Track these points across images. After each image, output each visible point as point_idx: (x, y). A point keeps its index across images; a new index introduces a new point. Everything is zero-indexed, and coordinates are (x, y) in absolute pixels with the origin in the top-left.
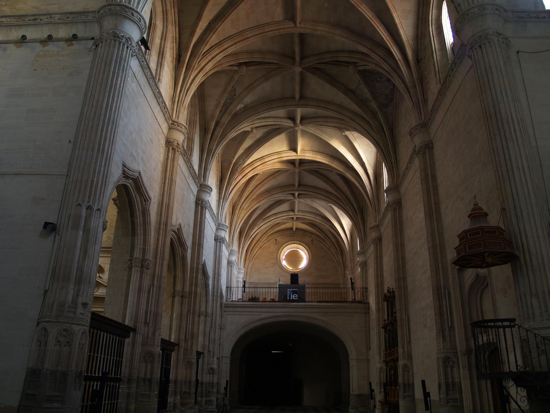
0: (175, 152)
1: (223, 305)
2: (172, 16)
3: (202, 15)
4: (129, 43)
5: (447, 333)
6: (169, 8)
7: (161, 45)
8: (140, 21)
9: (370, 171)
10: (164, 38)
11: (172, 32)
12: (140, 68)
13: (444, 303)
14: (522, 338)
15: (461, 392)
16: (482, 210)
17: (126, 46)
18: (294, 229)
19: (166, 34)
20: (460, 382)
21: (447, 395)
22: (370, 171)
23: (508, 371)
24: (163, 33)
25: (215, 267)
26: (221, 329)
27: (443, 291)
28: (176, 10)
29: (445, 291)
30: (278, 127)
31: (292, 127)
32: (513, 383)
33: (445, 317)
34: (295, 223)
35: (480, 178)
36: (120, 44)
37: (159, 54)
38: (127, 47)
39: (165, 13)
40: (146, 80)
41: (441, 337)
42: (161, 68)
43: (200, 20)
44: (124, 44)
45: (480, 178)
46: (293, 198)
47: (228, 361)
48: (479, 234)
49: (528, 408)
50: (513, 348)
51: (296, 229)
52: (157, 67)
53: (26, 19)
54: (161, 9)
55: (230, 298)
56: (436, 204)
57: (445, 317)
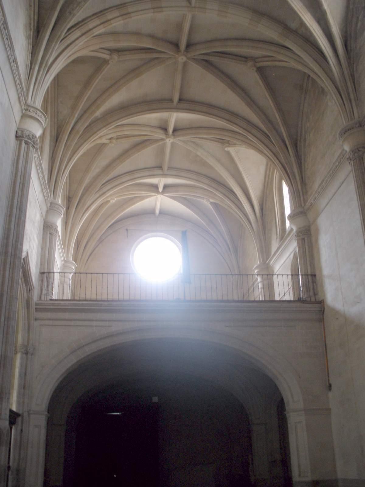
0: (28, 148)
1: (33, 307)
9: (336, 30)
18: (157, 212)
22: (336, 30)
25: (14, 192)
26: (27, 353)
30: (145, 138)
31: (162, 139)
34: (160, 197)
46: (163, 137)
47: (41, 421)
51: (161, 213)
55: (47, 294)
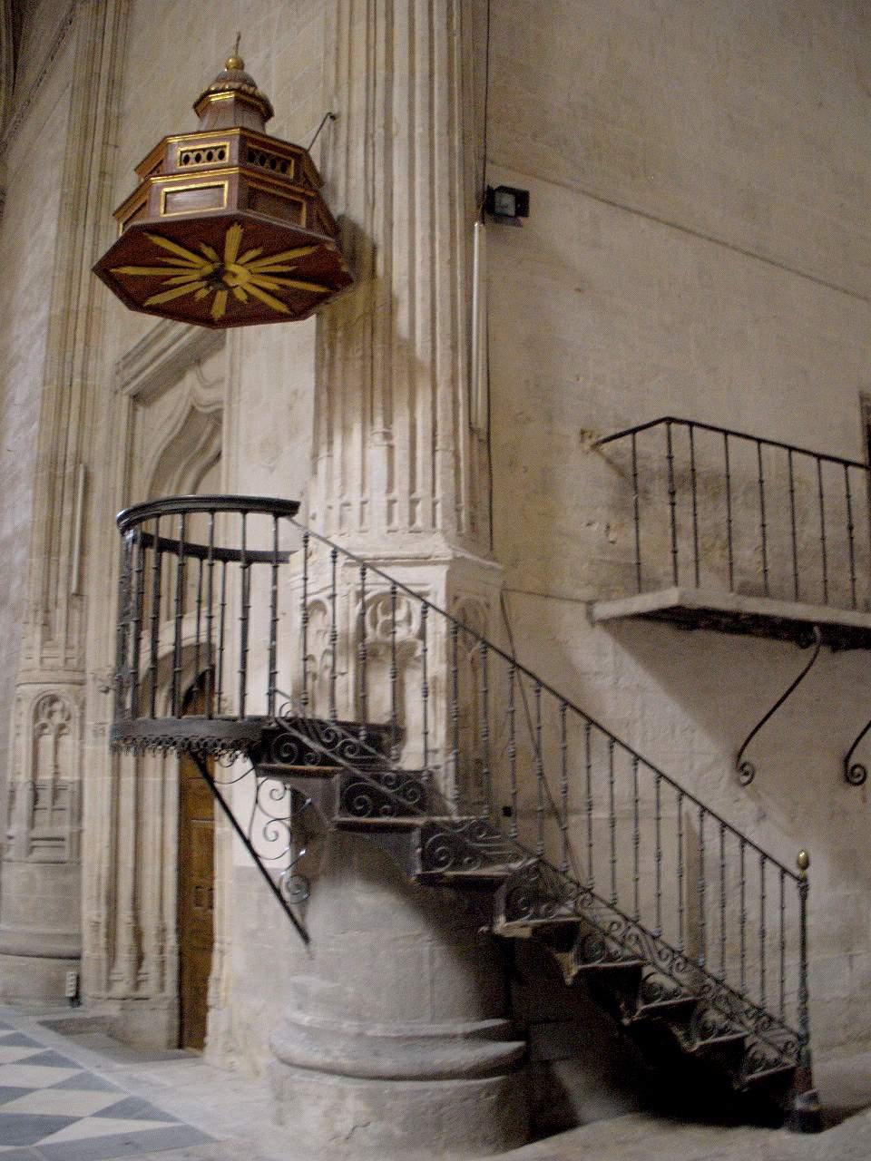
3: (111, 825)
5: (59, 615)
13: (67, 511)
14: (310, 599)
15: (78, 816)
16: (252, 84)
20: (81, 783)
21: (32, 824)
23: (236, 713)
27: (70, 469)
29: (76, 469)
32: (248, 765)
33: (64, 559)
35: (268, 56)
41: (38, 629)
45: (268, 56)
48: (222, 156)
49: (286, 862)
50: (266, 655)
56: (102, 174)
57: (64, 559)
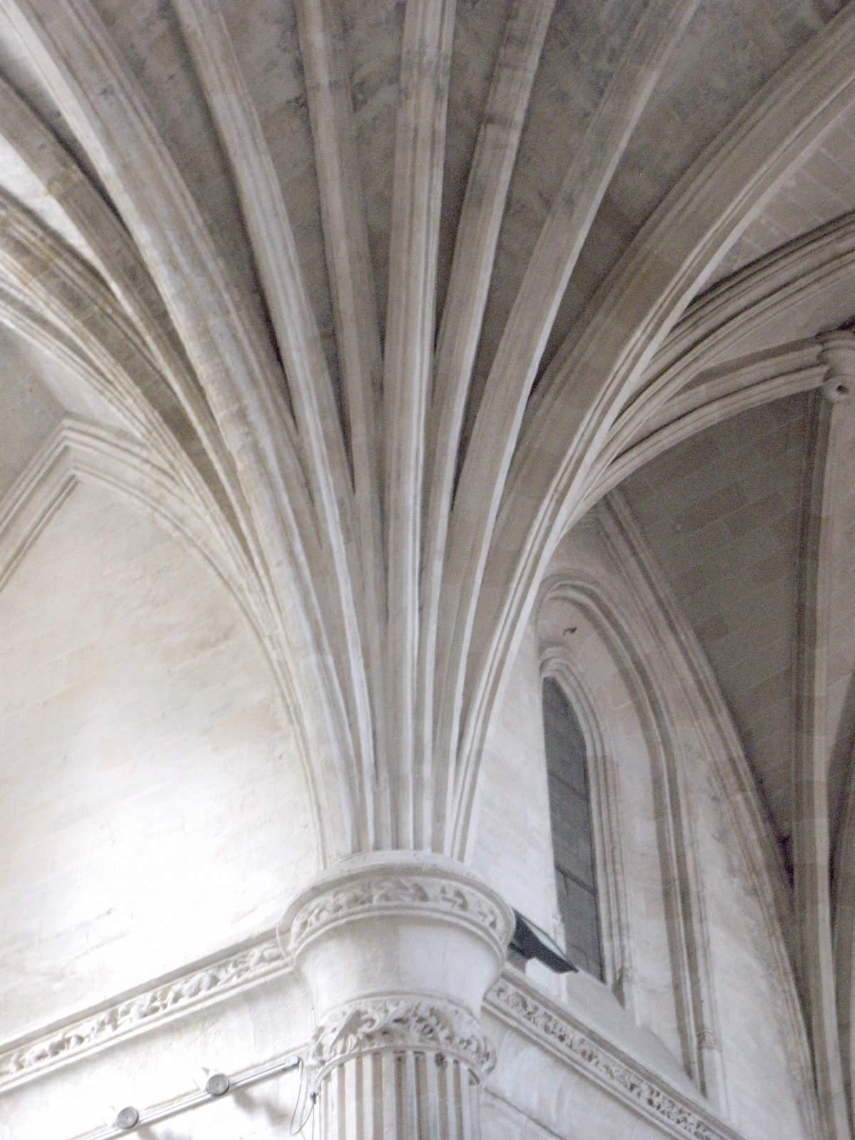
2: (677, 666)
4: (442, 1035)
6: (645, 646)
7: (662, 845)
8: (464, 906)
10: (667, 803)
11: (703, 743)
12: (563, 1074)
17: (431, 1055)
19: (672, 781)
24: (657, 783)
28: (689, 637)
36: (400, 1061)
37: (667, 895)
38: (440, 1060)
39: (637, 678)
40: (612, 1106)
42: (693, 969)
43: (813, 645)
44: (419, 1054)
52: (675, 968)
53: (29, 1056)
54: (614, 670)
